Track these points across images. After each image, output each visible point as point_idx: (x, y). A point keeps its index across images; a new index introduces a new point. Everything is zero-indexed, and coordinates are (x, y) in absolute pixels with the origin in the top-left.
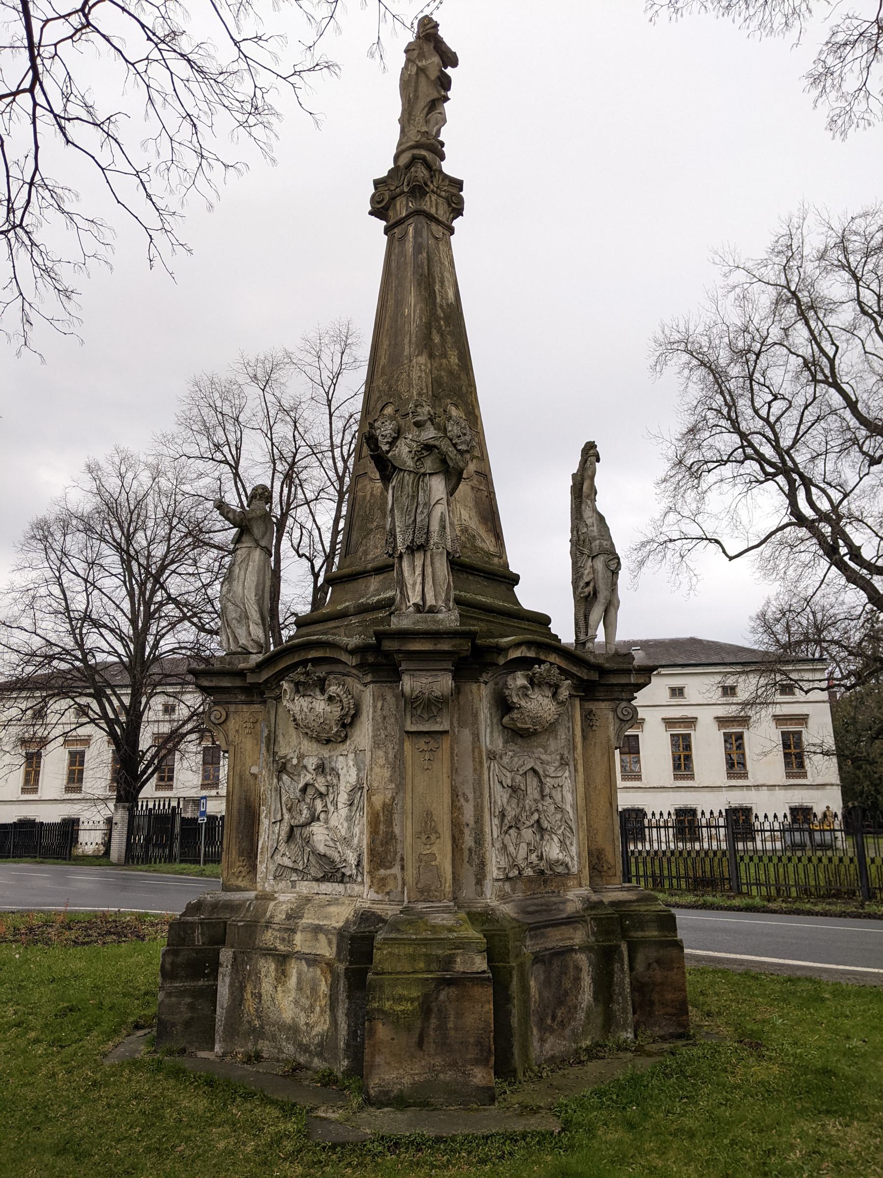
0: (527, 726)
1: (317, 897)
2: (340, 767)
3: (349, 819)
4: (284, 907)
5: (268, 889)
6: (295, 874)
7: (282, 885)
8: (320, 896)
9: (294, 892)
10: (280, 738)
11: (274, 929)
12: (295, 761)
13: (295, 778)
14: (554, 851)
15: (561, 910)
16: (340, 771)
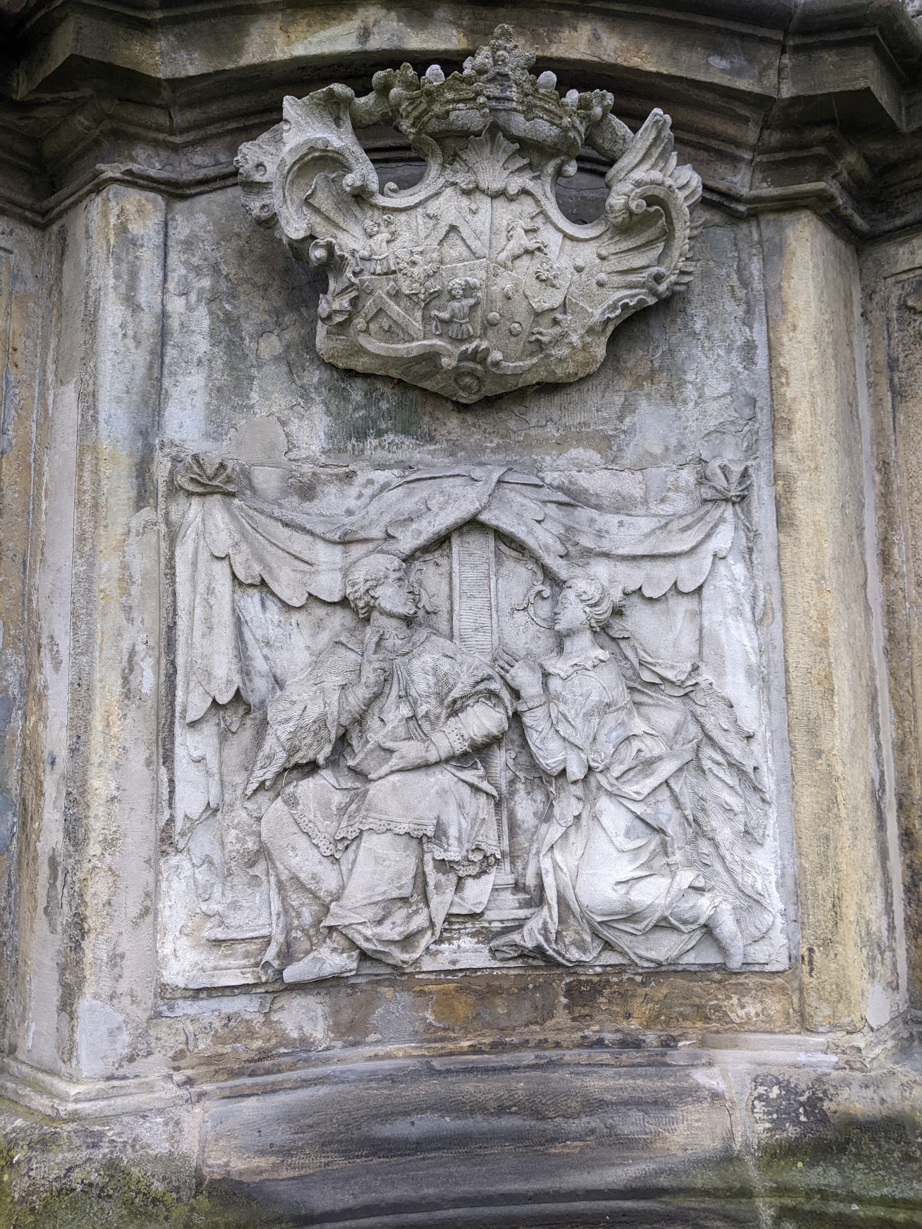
0: (415, 347)
14: (600, 865)
15: (627, 1143)
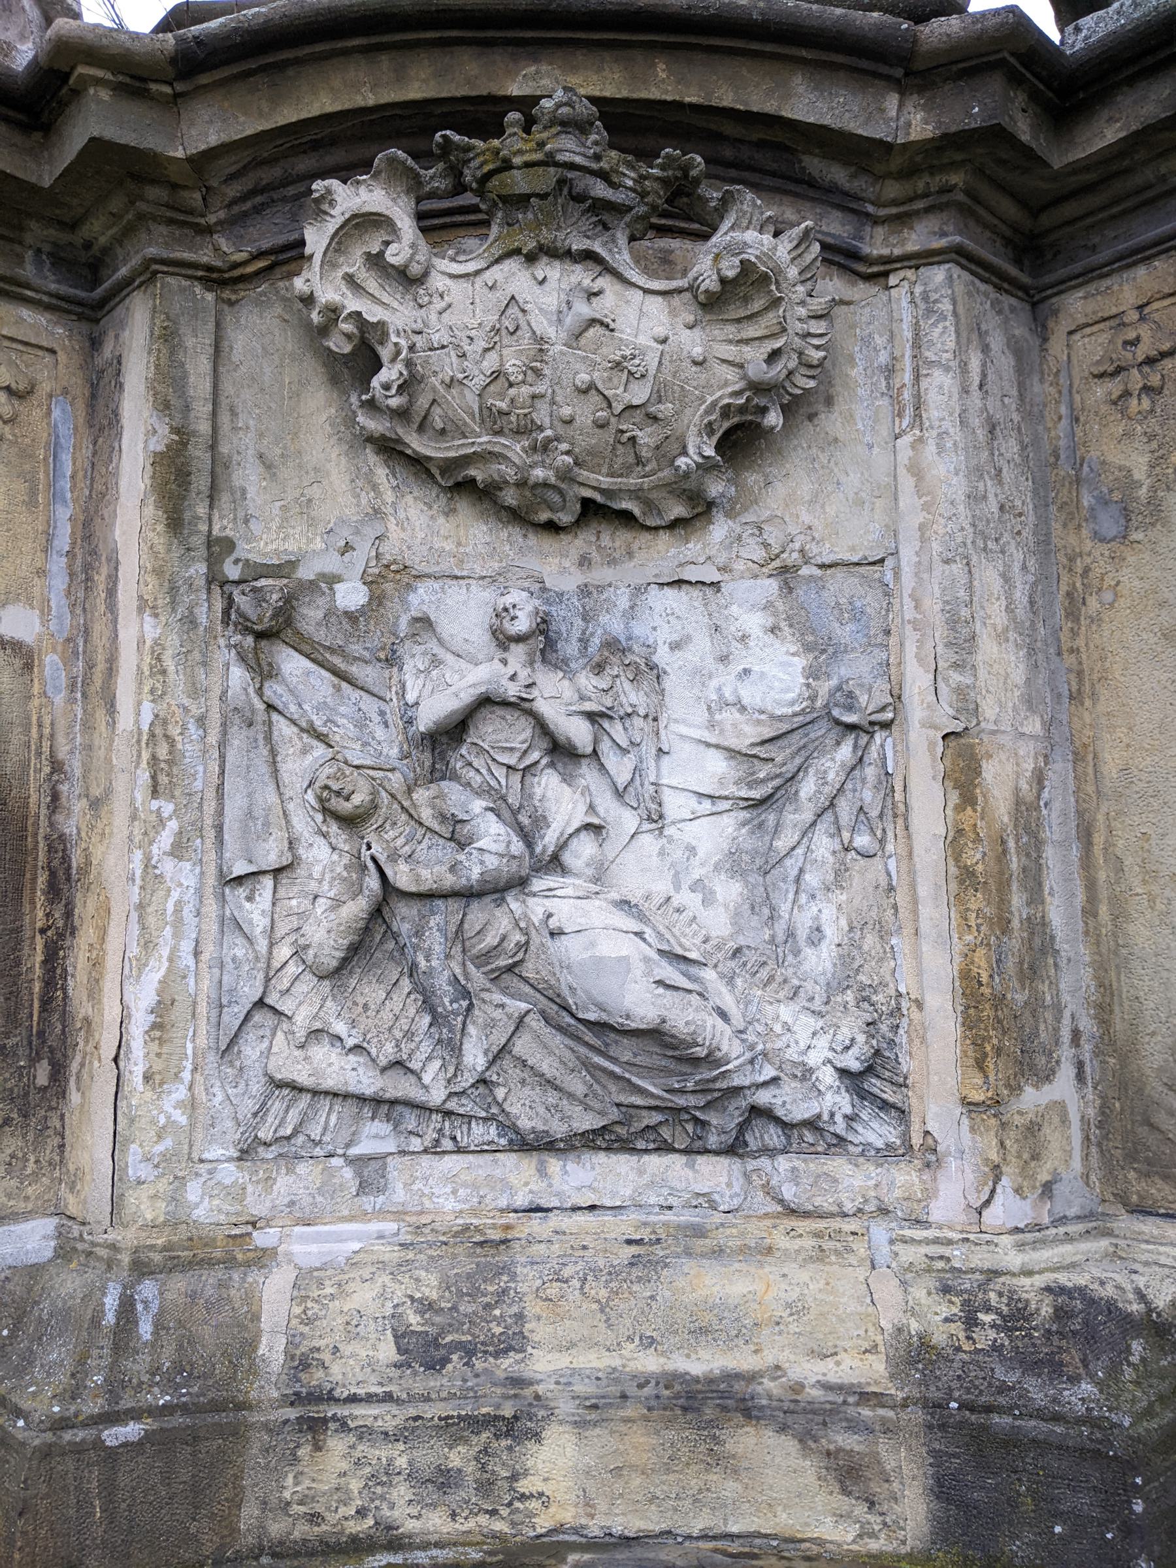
1: (535, 1225)
2: (664, 635)
3: (759, 868)
4: (363, 1297)
5: (205, 1207)
6: (380, 1127)
7: (297, 1183)
8: (555, 1221)
9: (381, 1214)
10: (248, 476)
11: (365, 1433)
12: (351, 595)
13: (367, 673)
16: (662, 656)
